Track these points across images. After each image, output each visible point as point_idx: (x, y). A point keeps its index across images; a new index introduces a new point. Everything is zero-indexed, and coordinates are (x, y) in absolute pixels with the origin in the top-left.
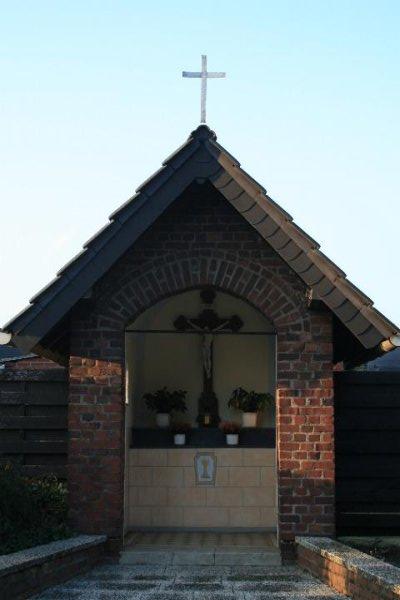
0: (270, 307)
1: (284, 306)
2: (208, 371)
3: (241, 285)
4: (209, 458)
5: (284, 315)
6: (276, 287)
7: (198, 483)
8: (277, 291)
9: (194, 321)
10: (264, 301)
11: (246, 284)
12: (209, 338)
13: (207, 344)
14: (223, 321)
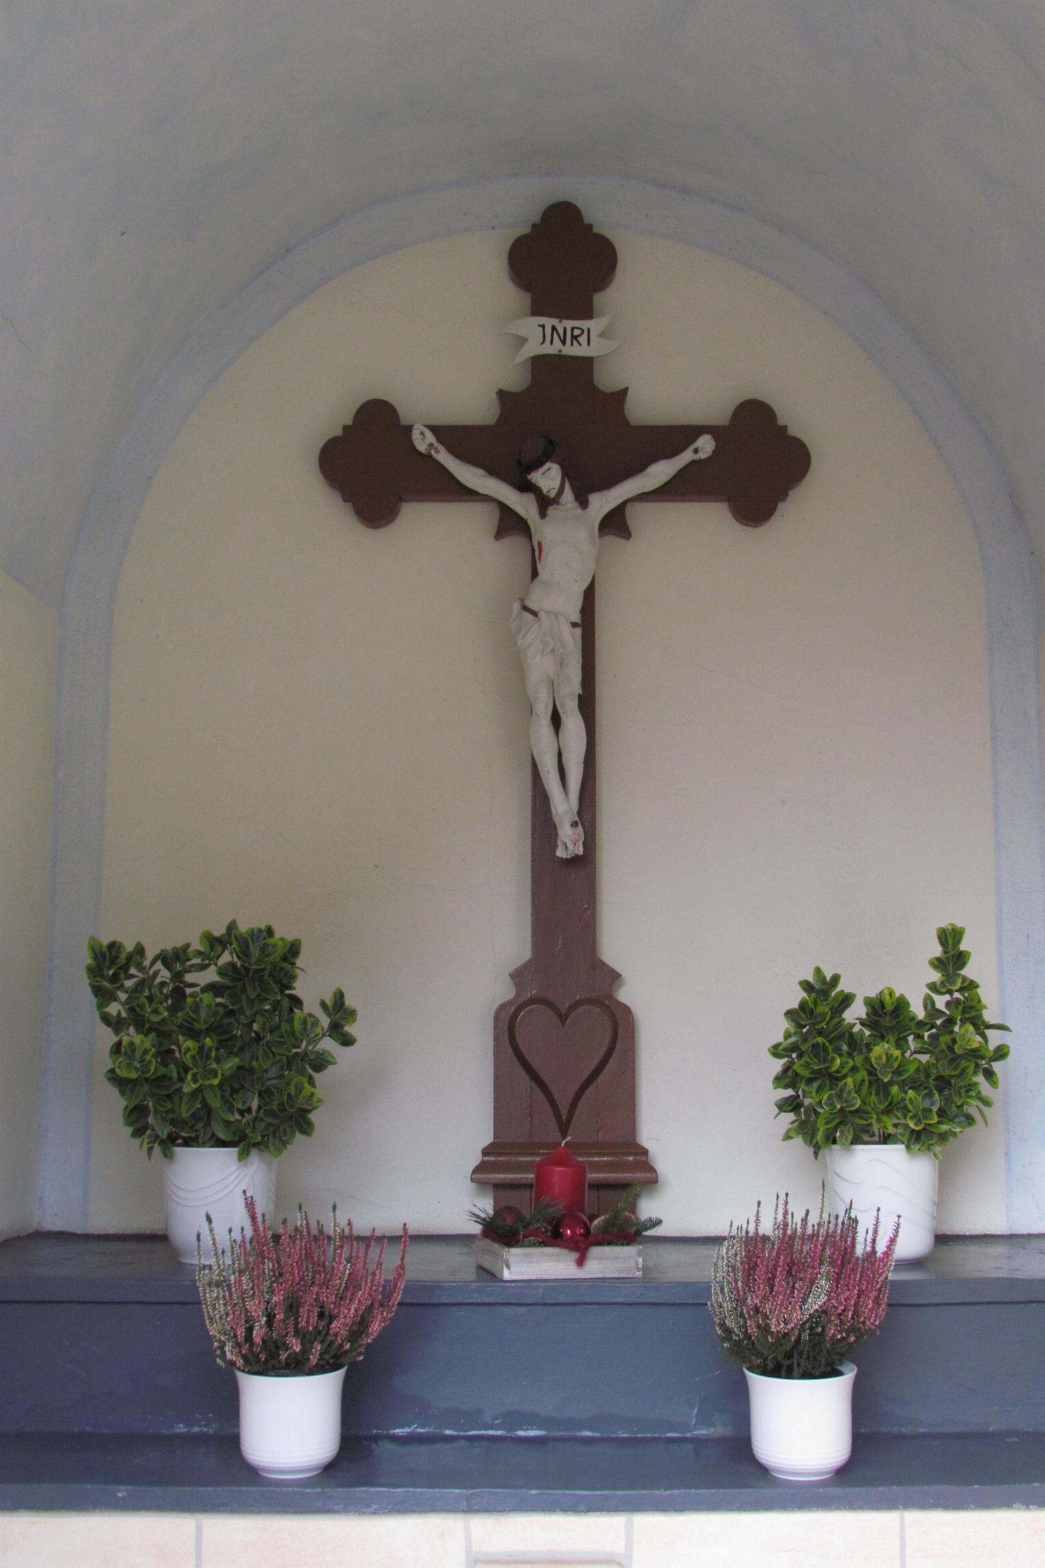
2: (563, 806)
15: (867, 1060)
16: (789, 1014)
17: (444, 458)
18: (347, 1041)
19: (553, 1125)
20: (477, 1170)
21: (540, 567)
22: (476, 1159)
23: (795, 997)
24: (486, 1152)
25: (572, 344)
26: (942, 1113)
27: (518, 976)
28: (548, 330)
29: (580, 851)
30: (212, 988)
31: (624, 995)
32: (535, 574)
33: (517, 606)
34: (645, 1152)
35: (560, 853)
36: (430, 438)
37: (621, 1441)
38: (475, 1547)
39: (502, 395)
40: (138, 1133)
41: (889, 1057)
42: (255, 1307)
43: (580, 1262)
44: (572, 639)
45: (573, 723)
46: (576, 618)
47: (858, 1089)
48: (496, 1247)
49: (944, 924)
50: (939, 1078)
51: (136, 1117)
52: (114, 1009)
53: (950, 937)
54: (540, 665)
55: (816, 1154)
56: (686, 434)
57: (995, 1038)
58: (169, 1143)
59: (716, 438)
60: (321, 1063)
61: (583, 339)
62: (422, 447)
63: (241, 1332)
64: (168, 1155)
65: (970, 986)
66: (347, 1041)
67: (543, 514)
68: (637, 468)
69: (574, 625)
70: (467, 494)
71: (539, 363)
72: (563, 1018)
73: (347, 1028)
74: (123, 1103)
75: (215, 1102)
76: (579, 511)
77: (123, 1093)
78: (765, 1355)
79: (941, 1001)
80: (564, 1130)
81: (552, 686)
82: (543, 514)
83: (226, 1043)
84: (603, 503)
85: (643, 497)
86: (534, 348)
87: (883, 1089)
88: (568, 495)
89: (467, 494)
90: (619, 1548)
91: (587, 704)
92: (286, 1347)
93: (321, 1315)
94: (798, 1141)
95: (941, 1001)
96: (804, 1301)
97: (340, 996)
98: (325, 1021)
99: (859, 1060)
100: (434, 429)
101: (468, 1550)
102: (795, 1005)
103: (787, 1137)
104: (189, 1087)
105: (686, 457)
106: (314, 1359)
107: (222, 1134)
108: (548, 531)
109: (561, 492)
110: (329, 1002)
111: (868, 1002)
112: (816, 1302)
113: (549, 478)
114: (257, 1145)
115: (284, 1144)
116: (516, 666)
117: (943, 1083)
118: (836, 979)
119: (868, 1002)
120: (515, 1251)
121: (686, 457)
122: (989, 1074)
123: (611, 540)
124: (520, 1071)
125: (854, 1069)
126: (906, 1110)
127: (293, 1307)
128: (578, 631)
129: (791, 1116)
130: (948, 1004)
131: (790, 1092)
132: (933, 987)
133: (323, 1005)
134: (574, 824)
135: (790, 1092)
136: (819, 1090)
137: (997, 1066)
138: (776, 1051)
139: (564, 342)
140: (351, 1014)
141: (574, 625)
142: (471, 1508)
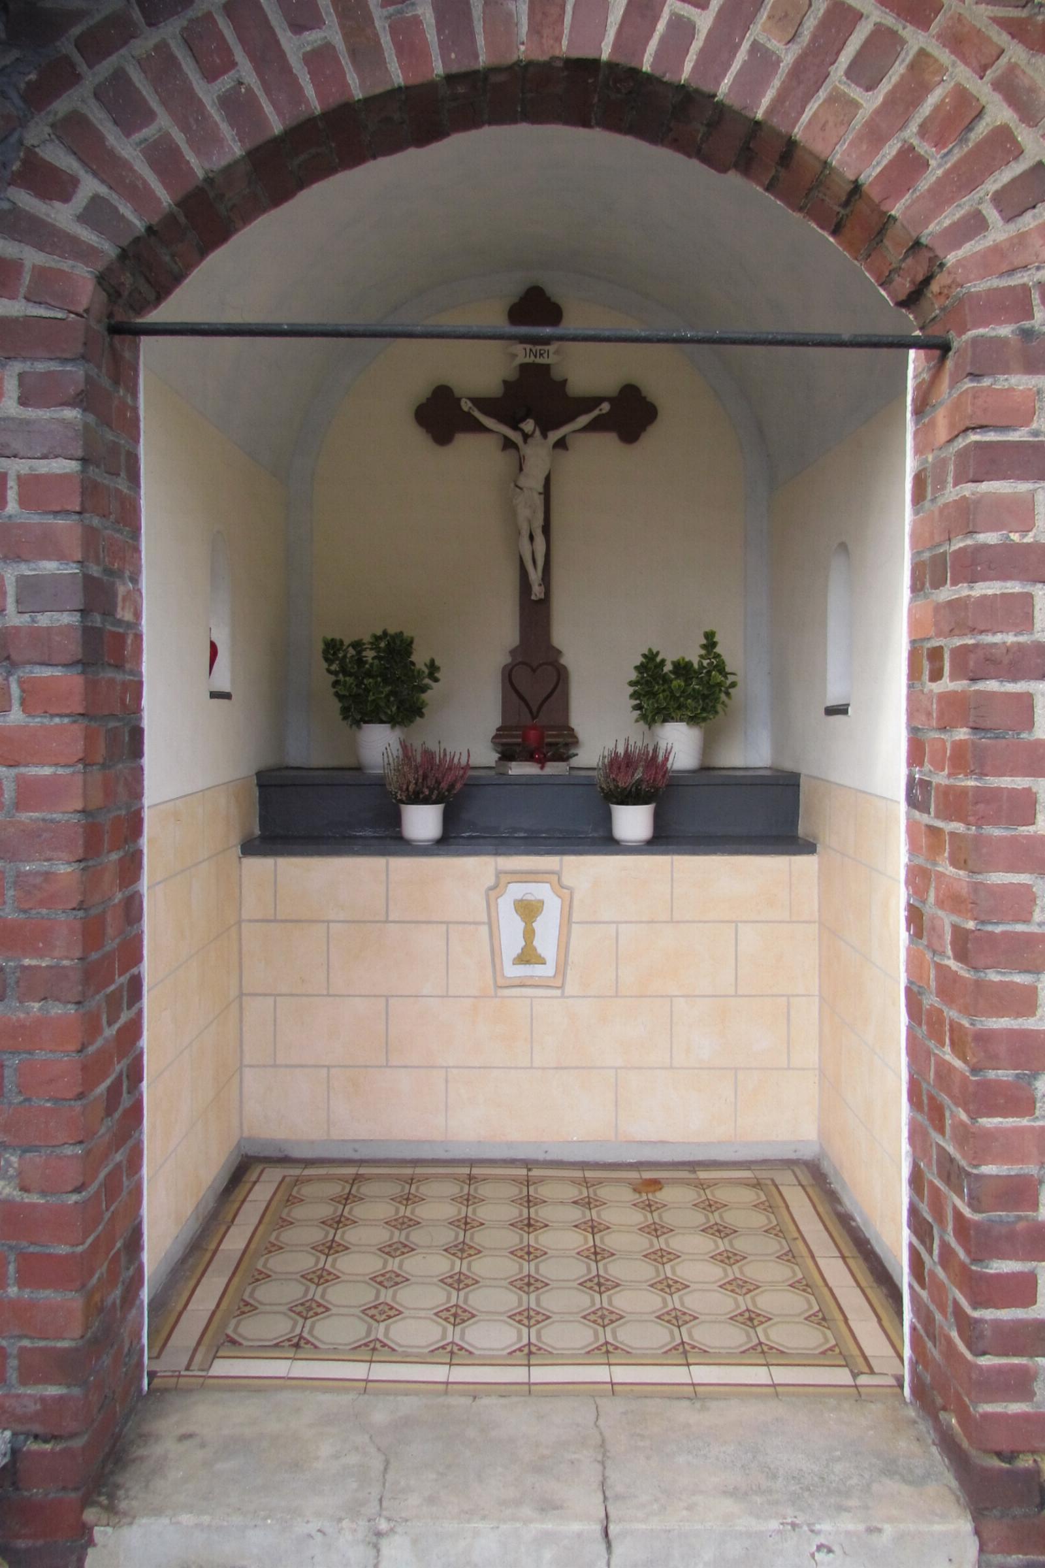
0: (925, 183)
1: (1006, 175)
2: (535, 576)
3: (762, 59)
4: (541, 891)
5: (999, 232)
6: (962, 74)
7: (502, 984)
8: (962, 97)
9: (483, 404)
10: (891, 150)
11: (788, 56)
12: (538, 454)
13: (533, 481)
14: (590, 403)
15: (670, 687)
16: (636, 668)
17: (477, 414)
18: (436, 680)
19: (529, 716)
20: (494, 738)
21: (524, 467)
22: (493, 733)
23: (639, 660)
24: (498, 730)
26: (703, 709)
27: (513, 652)
28: (528, 351)
29: (542, 596)
31: (563, 661)
32: (521, 469)
33: (512, 485)
34: (573, 730)
35: (533, 597)
36: (470, 404)
37: (559, 838)
38: (499, 868)
39: (505, 382)
40: (345, 718)
41: (679, 686)
42: (411, 777)
43: (542, 768)
44: (539, 501)
45: (540, 540)
46: (541, 490)
47: (665, 699)
48: (506, 763)
49: (707, 630)
50: (704, 695)
51: (346, 713)
52: (334, 667)
53: (709, 636)
54: (523, 513)
55: (650, 728)
56: (596, 401)
57: (731, 679)
58: (358, 723)
59: (610, 403)
60: (424, 689)
61: (545, 355)
62: (465, 409)
63: (405, 787)
64: (359, 727)
65: (717, 656)
66: (436, 680)
67: (525, 441)
68: (571, 418)
69: (540, 494)
70: (486, 430)
71: (524, 367)
72: (534, 671)
73: (436, 675)
74: (340, 705)
75: (382, 704)
76: (543, 441)
77: (340, 701)
79: (705, 662)
80: (534, 718)
81: (530, 522)
82: (525, 441)
83: (386, 681)
84: (554, 436)
85: (575, 431)
86: (522, 359)
87: (676, 699)
88: (538, 433)
89: (486, 430)
91: (546, 530)
92: (423, 793)
93: (436, 782)
94: (642, 722)
95: (705, 662)
96: (633, 775)
97: (432, 661)
98: (427, 671)
99: (666, 686)
100: (471, 400)
101: (496, 869)
102: (638, 664)
103: (637, 721)
104: (371, 698)
105: (596, 413)
106: (434, 797)
107: (384, 718)
108: (528, 450)
109: (534, 430)
110: (428, 662)
111: (673, 663)
112: (638, 775)
113: (529, 426)
114: (399, 723)
115: (412, 722)
116: (512, 513)
117: (705, 697)
118: (658, 653)
119: (673, 663)
120: (514, 763)
121: (596, 413)
122: (728, 694)
123: (559, 451)
124: (514, 695)
125: (664, 691)
126: (687, 708)
127: (425, 777)
129: (639, 712)
130: (708, 664)
131: (638, 702)
132: (701, 656)
133: (426, 665)
134: (540, 585)
135: (638, 702)
136: (648, 699)
137: (731, 690)
138: (631, 684)
139: (536, 356)
140: (438, 669)
141: (540, 494)
142: (497, 854)
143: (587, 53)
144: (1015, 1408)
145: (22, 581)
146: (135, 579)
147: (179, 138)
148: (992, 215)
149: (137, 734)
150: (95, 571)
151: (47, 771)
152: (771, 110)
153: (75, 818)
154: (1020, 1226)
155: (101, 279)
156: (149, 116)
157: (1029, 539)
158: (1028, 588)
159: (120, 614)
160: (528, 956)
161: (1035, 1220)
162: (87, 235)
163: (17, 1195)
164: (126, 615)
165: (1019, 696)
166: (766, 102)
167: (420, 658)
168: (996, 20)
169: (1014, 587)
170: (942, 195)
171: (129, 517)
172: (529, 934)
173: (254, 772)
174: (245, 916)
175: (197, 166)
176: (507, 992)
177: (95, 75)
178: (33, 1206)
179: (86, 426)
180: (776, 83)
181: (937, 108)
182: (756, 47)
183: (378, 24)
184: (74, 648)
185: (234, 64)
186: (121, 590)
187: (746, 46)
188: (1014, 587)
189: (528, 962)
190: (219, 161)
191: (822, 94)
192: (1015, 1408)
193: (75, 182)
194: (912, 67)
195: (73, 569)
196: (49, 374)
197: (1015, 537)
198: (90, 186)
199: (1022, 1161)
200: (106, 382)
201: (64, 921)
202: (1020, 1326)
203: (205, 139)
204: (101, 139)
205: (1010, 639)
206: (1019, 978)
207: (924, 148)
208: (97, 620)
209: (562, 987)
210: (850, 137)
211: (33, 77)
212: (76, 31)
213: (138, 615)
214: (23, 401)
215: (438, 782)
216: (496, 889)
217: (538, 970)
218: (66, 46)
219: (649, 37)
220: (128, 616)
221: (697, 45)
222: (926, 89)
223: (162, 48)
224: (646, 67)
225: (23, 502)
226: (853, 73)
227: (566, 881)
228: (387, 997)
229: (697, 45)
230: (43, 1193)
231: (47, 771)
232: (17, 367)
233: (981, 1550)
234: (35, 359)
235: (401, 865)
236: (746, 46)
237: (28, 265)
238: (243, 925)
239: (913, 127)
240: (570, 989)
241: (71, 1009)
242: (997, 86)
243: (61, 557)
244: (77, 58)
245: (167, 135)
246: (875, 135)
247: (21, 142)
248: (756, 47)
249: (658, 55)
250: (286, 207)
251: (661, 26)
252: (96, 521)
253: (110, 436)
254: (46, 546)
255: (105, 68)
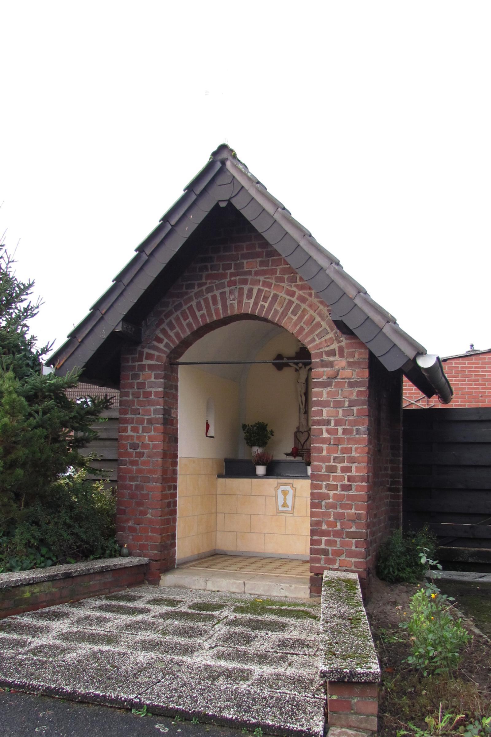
0: (304, 333)
3: (276, 311)
4: (288, 488)
5: (317, 341)
6: (311, 312)
10: (298, 327)
11: (281, 311)
18: (273, 435)
25: (37, 340)
30: (256, 429)
45: (304, 397)
51: (247, 443)
58: (252, 446)
60: (270, 438)
64: (251, 447)
66: (273, 435)
78: (420, 544)
88: (303, 367)
90: (292, 482)
97: (272, 430)
128: (305, 385)
140: (273, 432)
142: (277, 478)
143: (246, 312)
144: (317, 565)
145: (154, 409)
146: (177, 409)
147: (180, 331)
148: (316, 339)
149: (177, 438)
150: (166, 408)
151: (157, 443)
152: (278, 321)
153: (161, 451)
154: (319, 530)
155: (167, 357)
156: (175, 328)
157: (322, 399)
158: (322, 409)
159: (172, 415)
160: (284, 505)
161: (321, 529)
162: (165, 349)
163: (151, 517)
164: (173, 415)
165: (320, 429)
166: (277, 319)
167: (269, 429)
168: (318, 301)
169: (320, 408)
170: (307, 335)
171: (176, 398)
172: (285, 499)
173: (224, 458)
174: (218, 493)
175: (183, 336)
176: (279, 514)
177: (167, 321)
178: (153, 519)
179: (165, 383)
180: (279, 316)
181: (307, 319)
182: (275, 309)
183: (212, 309)
184: (162, 421)
185: (188, 318)
186: (173, 411)
187: (273, 309)
188: (320, 408)
189: (285, 507)
190: (186, 335)
191: (287, 317)
192: (317, 565)
193: (163, 340)
194: (302, 311)
195: (162, 407)
196: (159, 373)
197: (319, 399)
198: (166, 340)
199: (319, 517)
200: (169, 373)
201: (159, 469)
202: (319, 549)
203: (184, 331)
204: (167, 332)
205: (318, 418)
206: (319, 483)
207: (304, 326)
208: (167, 416)
209: (293, 513)
210: (291, 325)
211: (157, 322)
212: (164, 314)
213: (177, 416)
214: (155, 378)
215: (263, 460)
216: (277, 488)
217: (287, 509)
218: (162, 316)
219: (257, 309)
220: (174, 416)
221: (265, 310)
222: (305, 315)
223: (177, 315)
224: (256, 315)
225: (154, 396)
226: (292, 313)
227: (294, 486)
228: (251, 515)
229: (265, 310)
230: (155, 517)
231: (157, 443)
232: (154, 372)
233: (310, 592)
234: (157, 371)
235: (254, 481)
236: (273, 309)
237: (156, 355)
238: (218, 495)
239: (302, 323)
240: (295, 514)
241: (160, 484)
242: (317, 314)
243: (160, 405)
244: (164, 318)
245: (178, 331)
246: (296, 325)
247: (155, 333)
248: (275, 309)
249: (258, 312)
250: (202, 338)
251: (259, 307)
252: (167, 399)
253: (171, 383)
254: (158, 404)
255: (168, 320)
